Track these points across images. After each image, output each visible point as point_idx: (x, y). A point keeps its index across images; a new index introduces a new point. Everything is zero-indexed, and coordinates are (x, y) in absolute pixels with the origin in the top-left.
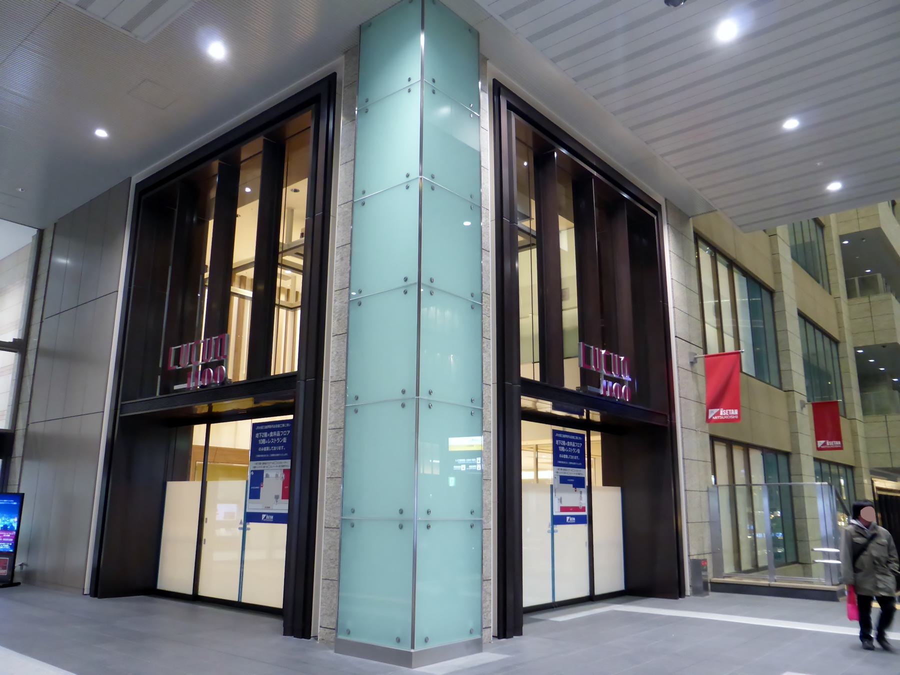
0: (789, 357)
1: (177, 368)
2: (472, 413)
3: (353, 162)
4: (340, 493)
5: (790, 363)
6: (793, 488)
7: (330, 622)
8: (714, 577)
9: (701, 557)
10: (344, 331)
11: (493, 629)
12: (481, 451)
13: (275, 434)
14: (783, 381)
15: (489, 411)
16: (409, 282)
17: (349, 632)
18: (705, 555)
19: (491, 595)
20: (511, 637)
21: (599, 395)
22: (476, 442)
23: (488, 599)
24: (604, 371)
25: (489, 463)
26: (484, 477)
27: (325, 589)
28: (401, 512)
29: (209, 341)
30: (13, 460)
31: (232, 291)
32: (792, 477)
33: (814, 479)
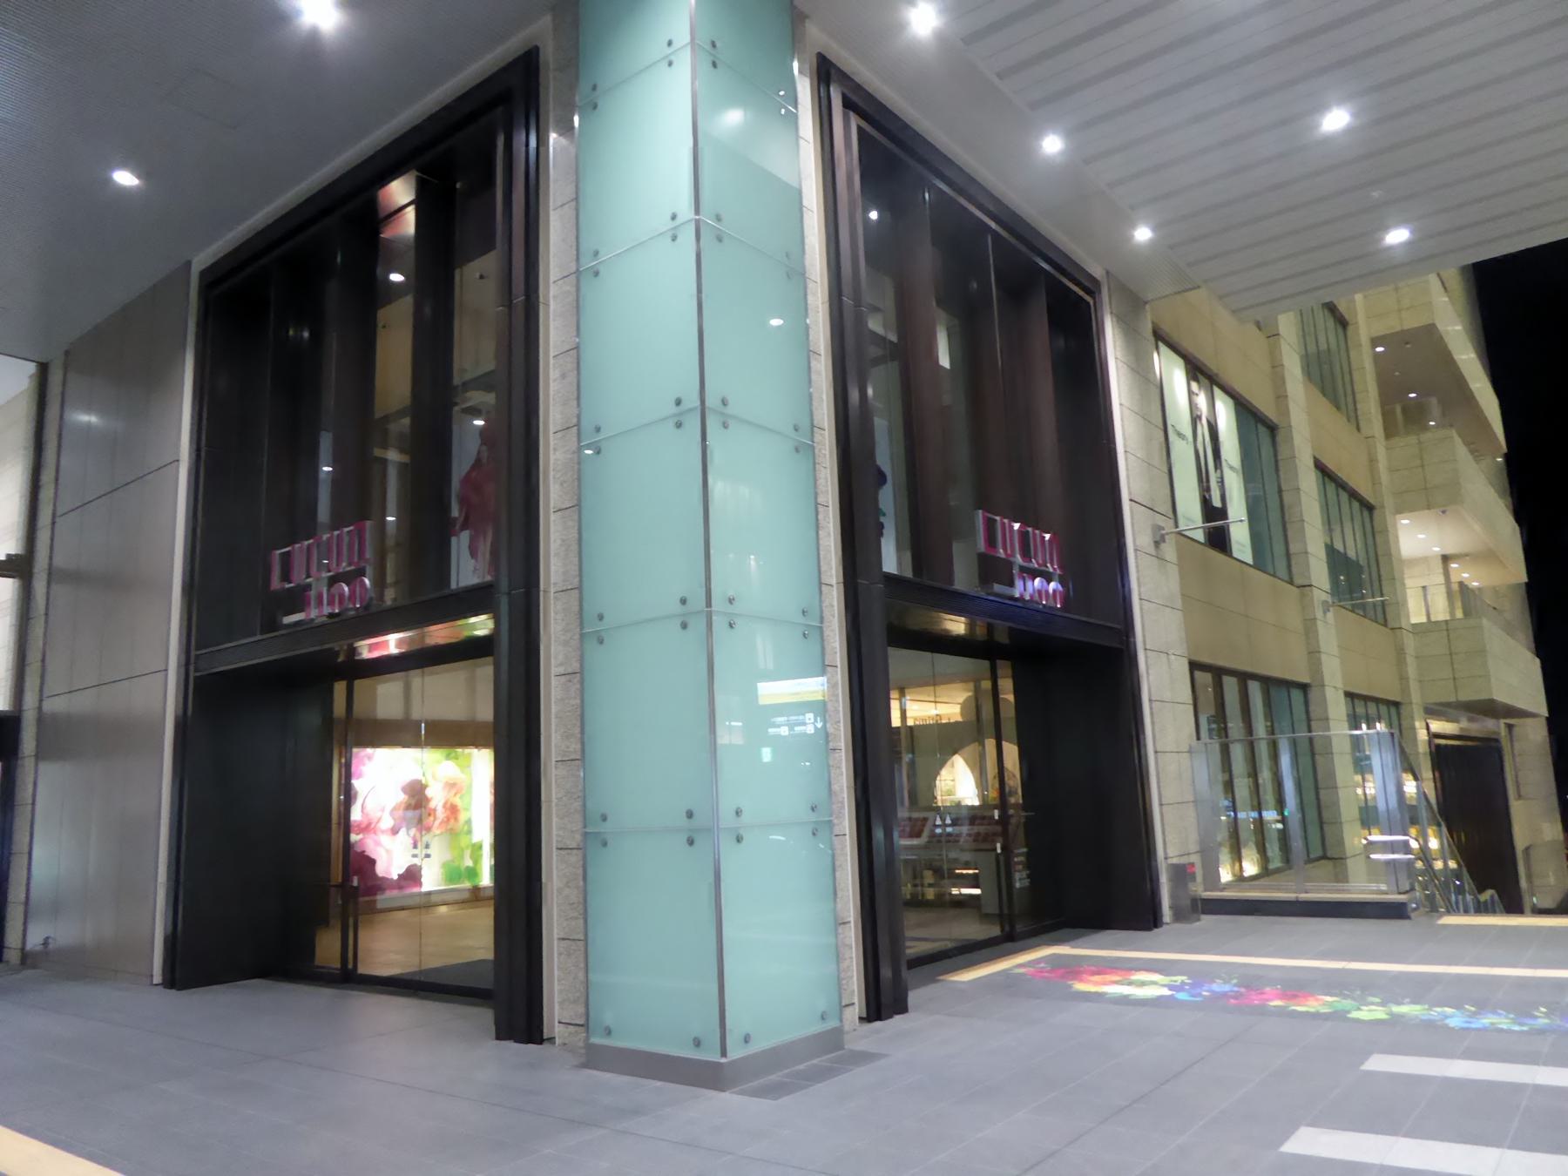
0: (1302, 530)
1: (287, 586)
2: (804, 634)
3: (574, 203)
4: (580, 787)
5: (1305, 543)
6: (1315, 741)
7: (574, 1013)
8: (1206, 890)
9: (1184, 860)
10: (576, 502)
11: (857, 1007)
12: (824, 700)
14: (1295, 570)
15: (832, 631)
16: (686, 405)
17: (608, 1032)
18: (1191, 856)
19: (851, 948)
20: (891, 1017)
21: (1012, 598)
22: (814, 687)
23: (847, 956)
24: (1019, 559)
25: (837, 720)
26: (831, 745)
27: (563, 956)
28: (690, 815)
29: (338, 535)
30: (20, 762)
32: (1313, 724)
33: (1346, 725)
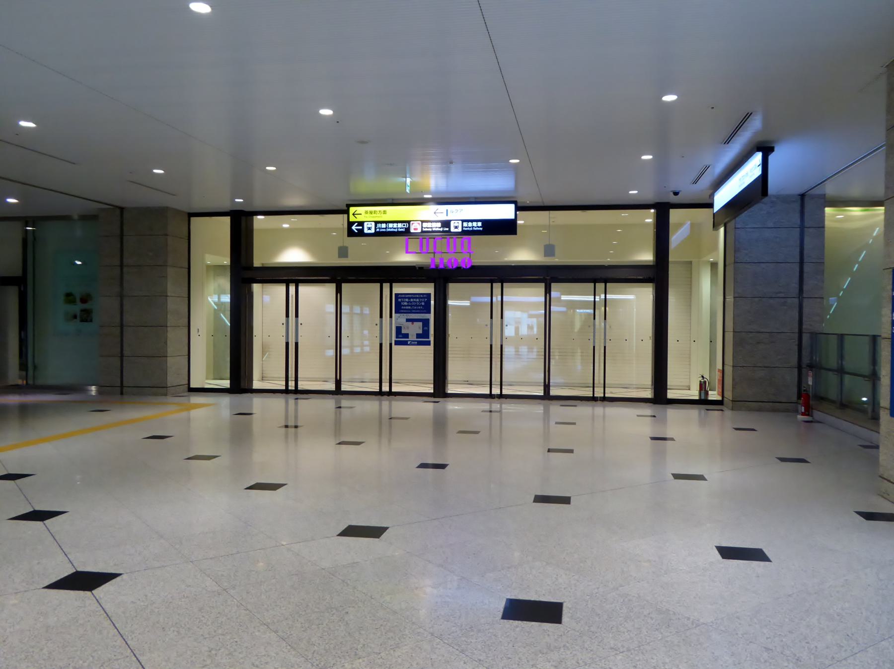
13: (415, 300)
31: (526, 334)
